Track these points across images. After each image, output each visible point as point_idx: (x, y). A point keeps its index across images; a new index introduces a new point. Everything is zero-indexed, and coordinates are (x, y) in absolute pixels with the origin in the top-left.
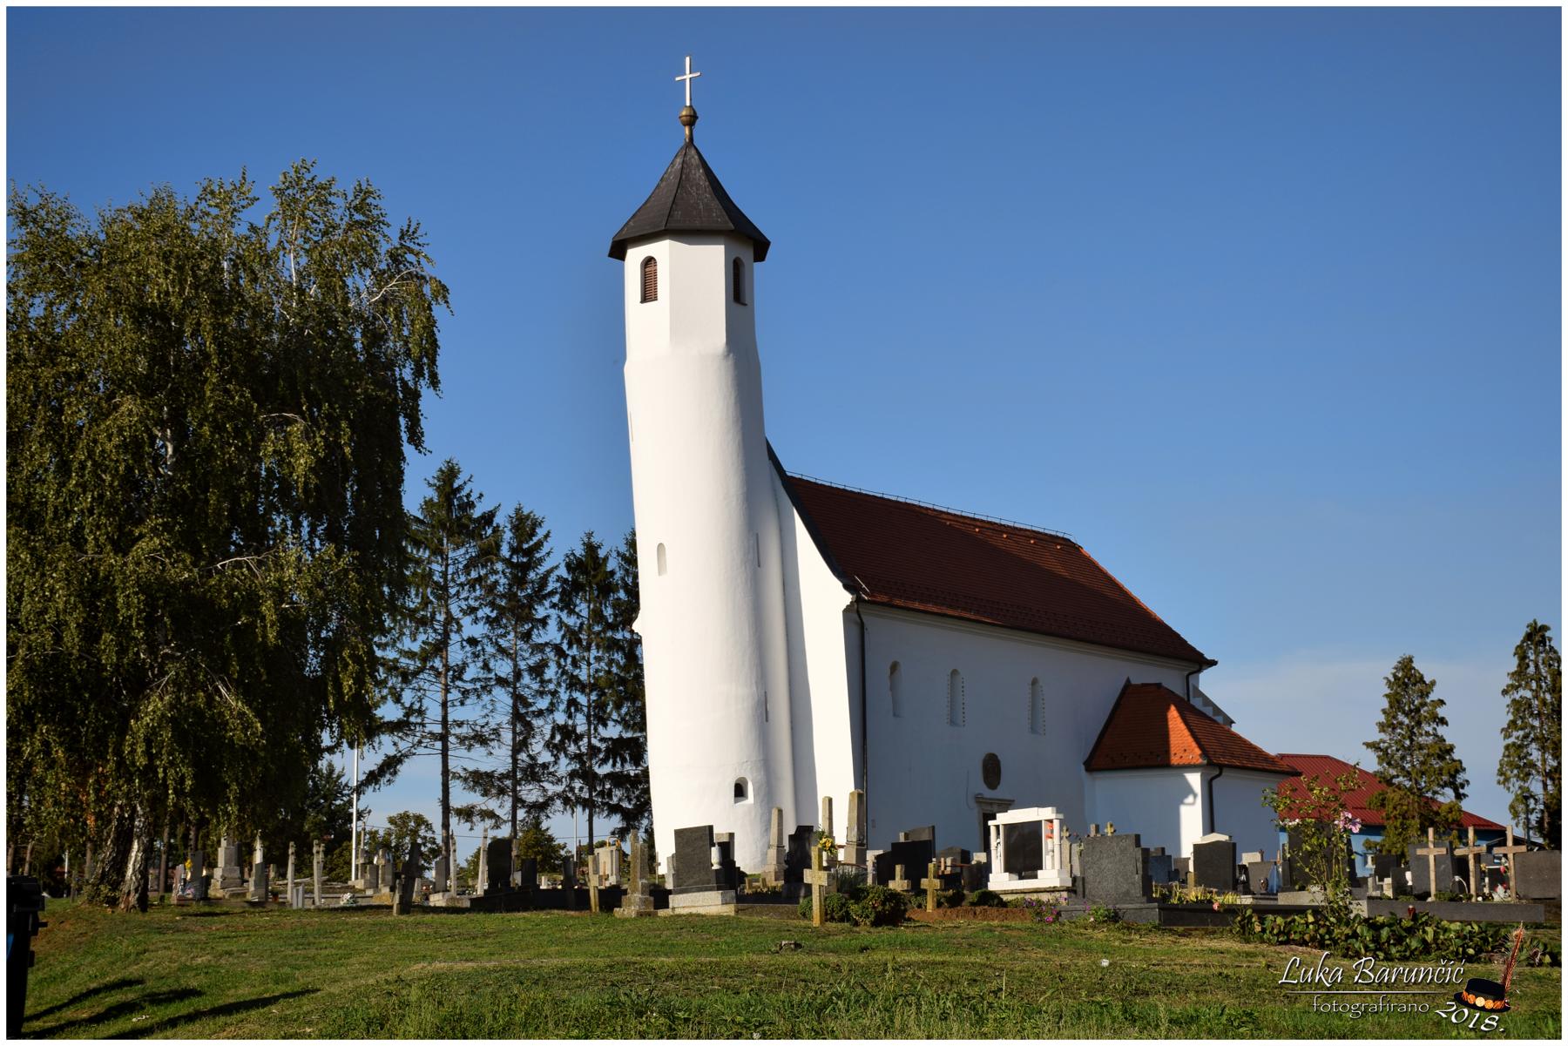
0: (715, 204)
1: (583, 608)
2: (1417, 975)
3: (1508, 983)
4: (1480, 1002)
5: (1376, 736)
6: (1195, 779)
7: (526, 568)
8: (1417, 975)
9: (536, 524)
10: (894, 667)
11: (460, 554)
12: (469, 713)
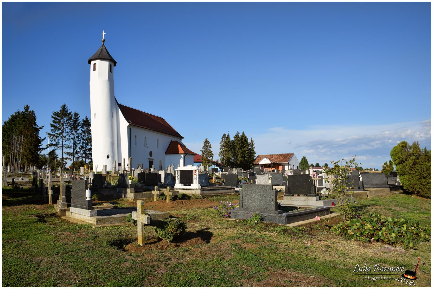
0: (107, 55)
1: (85, 128)
4: (409, 277)
5: (202, 149)
6: (182, 156)
7: (77, 121)
9: (78, 114)
10: (136, 136)
11: (66, 119)
12: (67, 143)
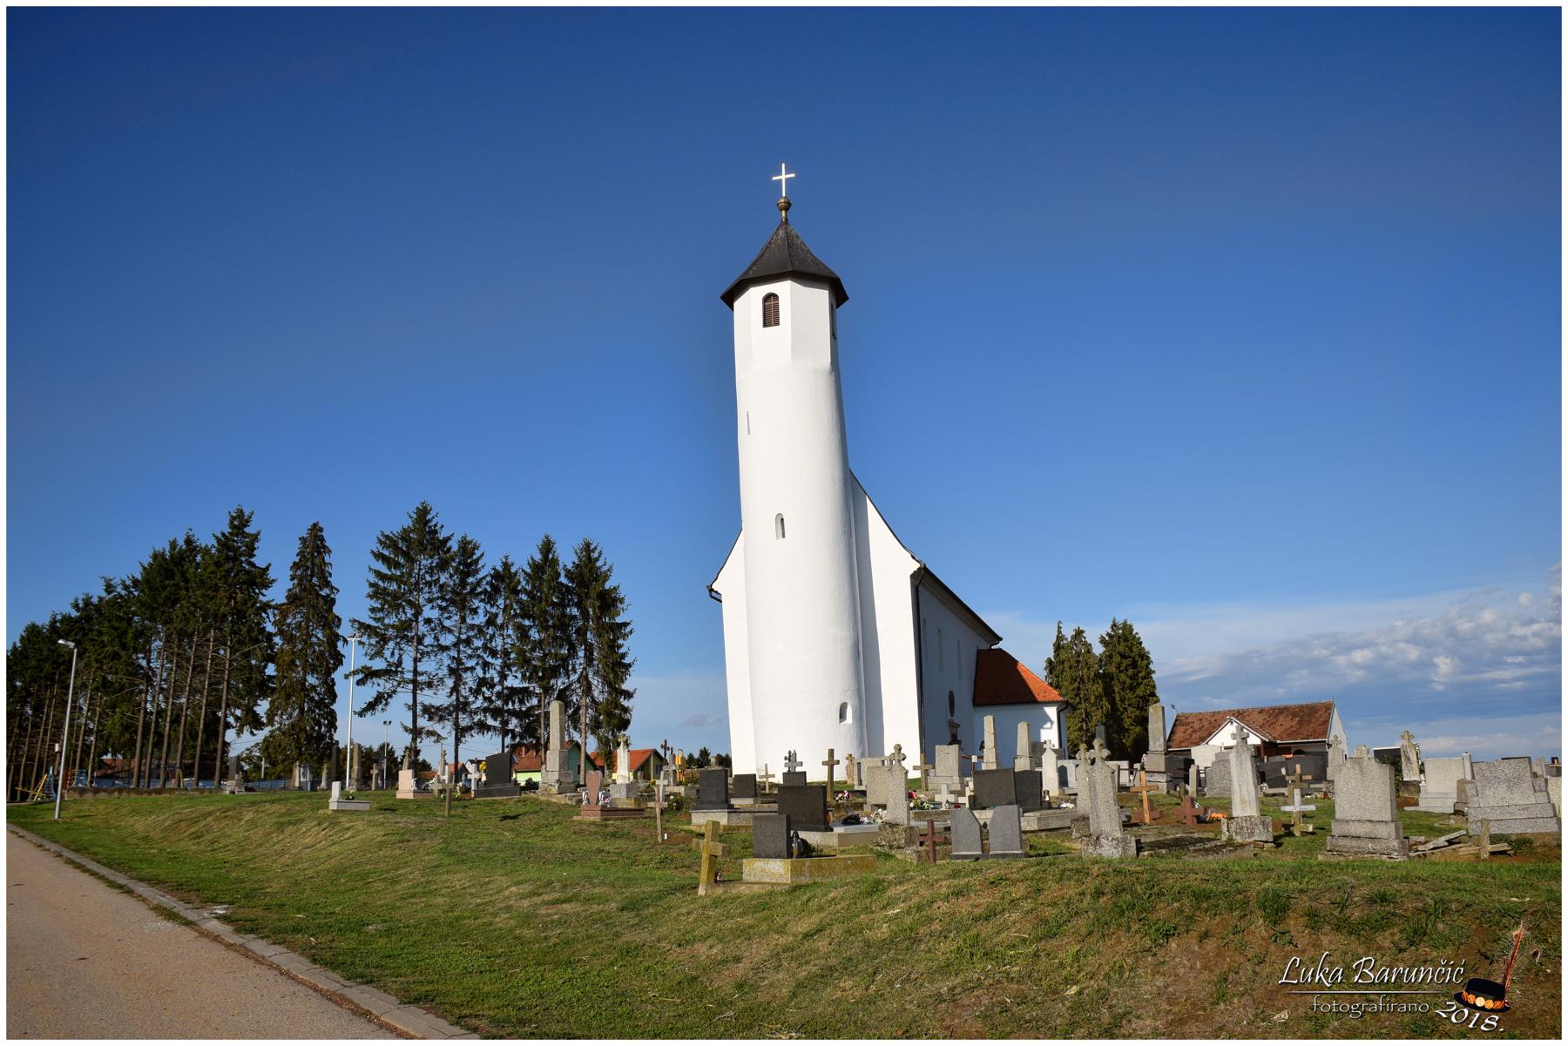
2: (1390, 974)
4: (1480, 1002)
6: (1052, 712)
8: (1390, 974)
9: (476, 547)
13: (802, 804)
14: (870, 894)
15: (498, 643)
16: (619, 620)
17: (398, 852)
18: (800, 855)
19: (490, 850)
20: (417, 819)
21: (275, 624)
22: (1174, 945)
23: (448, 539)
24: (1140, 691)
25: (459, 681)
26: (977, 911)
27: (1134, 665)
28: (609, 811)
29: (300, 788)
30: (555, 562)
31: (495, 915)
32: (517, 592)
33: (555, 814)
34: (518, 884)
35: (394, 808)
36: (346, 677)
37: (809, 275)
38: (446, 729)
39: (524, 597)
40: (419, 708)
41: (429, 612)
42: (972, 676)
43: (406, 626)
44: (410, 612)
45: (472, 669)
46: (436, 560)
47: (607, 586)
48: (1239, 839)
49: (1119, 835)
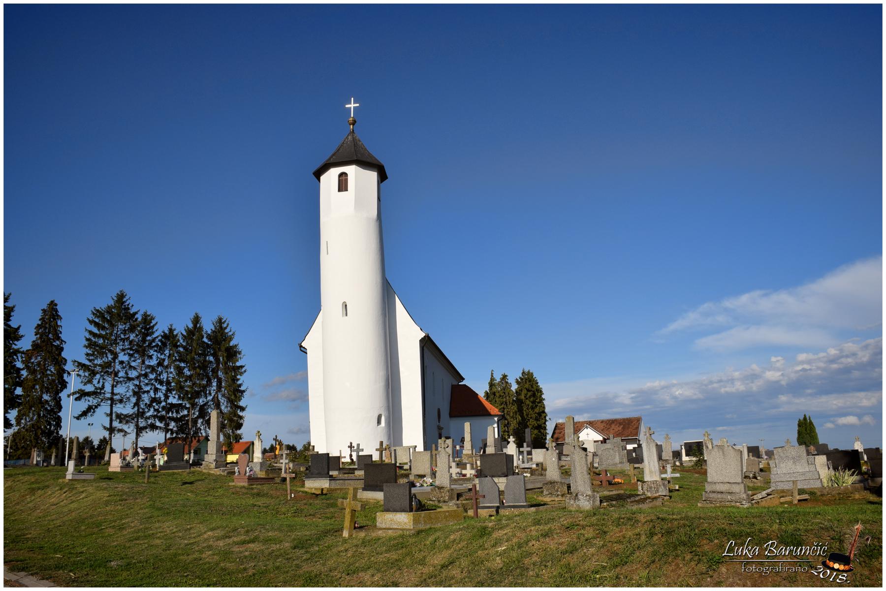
3: (852, 556)
4: (836, 566)
9: (153, 318)
13: (381, 473)
14: (481, 536)
15: (164, 376)
16: (238, 364)
17: (120, 507)
18: (418, 510)
19: (184, 506)
20: (130, 485)
21: (23, 362)
22: (724, 570)
23: (136, 313)
24: (537, 410)
25: (139, 399)
26: (562, 547)
27: (534, 395)
28: (252, 479)
29: (37, 464)
30: (201, 329)
31: (201, 552)
32: (177, 346)
33: (215, 481)
34: (212, 529)
35: (110, 477)
36: (69, 396)
37: (366, 163)
38: (130, 428)
39: (181, 349)
40: (114, 415)
41: (123, 357)
42: (451, 401)
43: (108, 365)
44: (110, 357)
45: (148, 392)
46: (128, 326)
47: (231, 344)
48: (649, 494)
49: (590, 493)
